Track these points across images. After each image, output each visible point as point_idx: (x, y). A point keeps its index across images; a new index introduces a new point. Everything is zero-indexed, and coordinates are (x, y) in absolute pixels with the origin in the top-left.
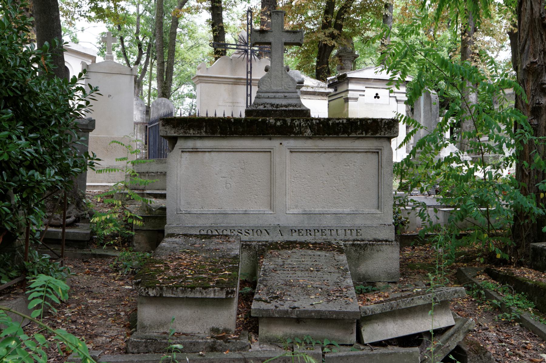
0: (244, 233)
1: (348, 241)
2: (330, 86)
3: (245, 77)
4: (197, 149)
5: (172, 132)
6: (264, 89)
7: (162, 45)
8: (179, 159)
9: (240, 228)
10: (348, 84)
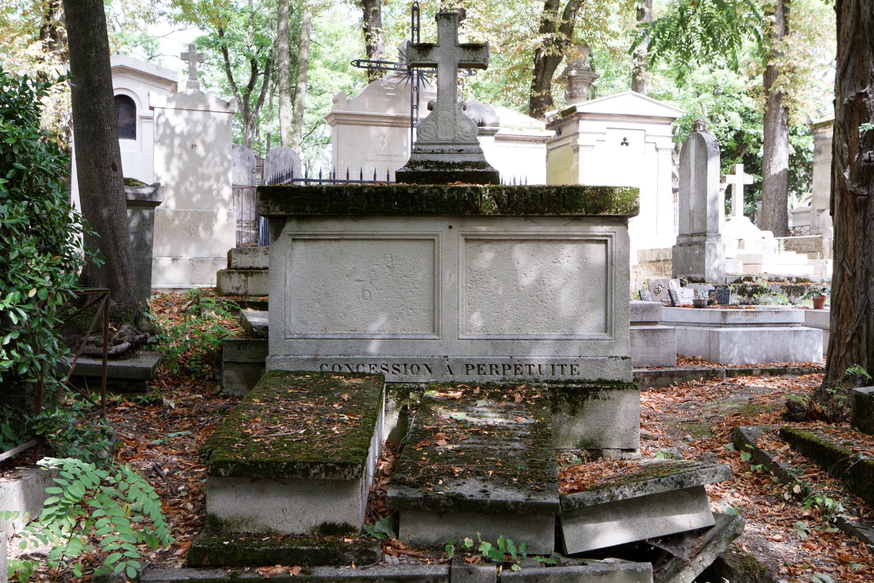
0: (391, 370)
1: (558, 382)
2: (549, 126)
3: (409, 115)
4: (317, 235)
5: (288, 205)
6: (426, 138)
7: (278, 65)
8: (289, 251)
9: (384, 362)
10: (578, 122)
